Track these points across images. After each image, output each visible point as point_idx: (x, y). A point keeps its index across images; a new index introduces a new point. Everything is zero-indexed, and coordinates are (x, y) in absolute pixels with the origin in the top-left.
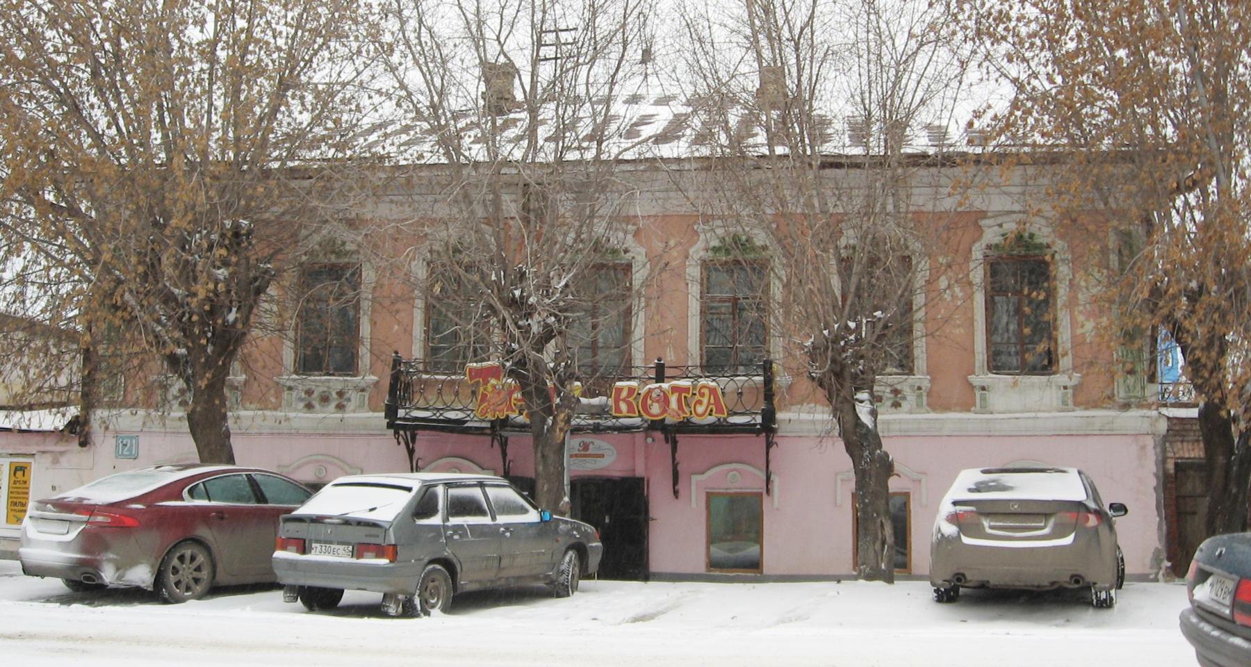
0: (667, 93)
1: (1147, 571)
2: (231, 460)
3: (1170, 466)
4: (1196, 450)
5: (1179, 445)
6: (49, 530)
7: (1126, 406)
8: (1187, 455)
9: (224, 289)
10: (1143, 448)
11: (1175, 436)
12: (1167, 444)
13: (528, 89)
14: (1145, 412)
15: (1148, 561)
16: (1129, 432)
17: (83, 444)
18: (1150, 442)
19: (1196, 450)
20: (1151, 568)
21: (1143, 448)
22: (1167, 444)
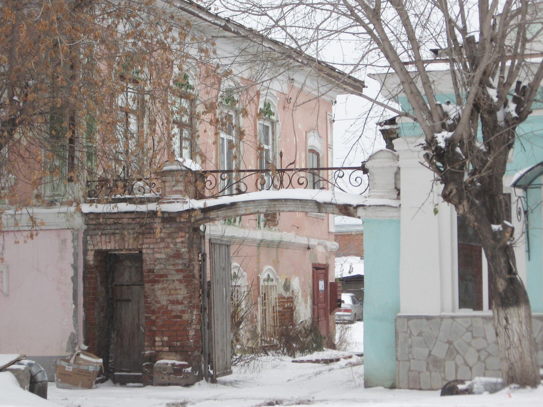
0: (261, 96)
1: (64, 354)
2: (511, 222)
3: (91, 257)
4: (113, 242)
5: (98, 238)
6: (228, 328)
7: (51, 204)
8: (104, 248)
9: (190, 53)
10: (64, 241)
11: (95, 229)
12: (88, 237)
13: (236, 35)
14: (64, 209)
15: (65, 345)
16: (52, 228)
17: (362, 234)
18: (69, 235)
19: (113, 242)
20: (67, 351)
21: (64, 241)
22: (88, 237)
